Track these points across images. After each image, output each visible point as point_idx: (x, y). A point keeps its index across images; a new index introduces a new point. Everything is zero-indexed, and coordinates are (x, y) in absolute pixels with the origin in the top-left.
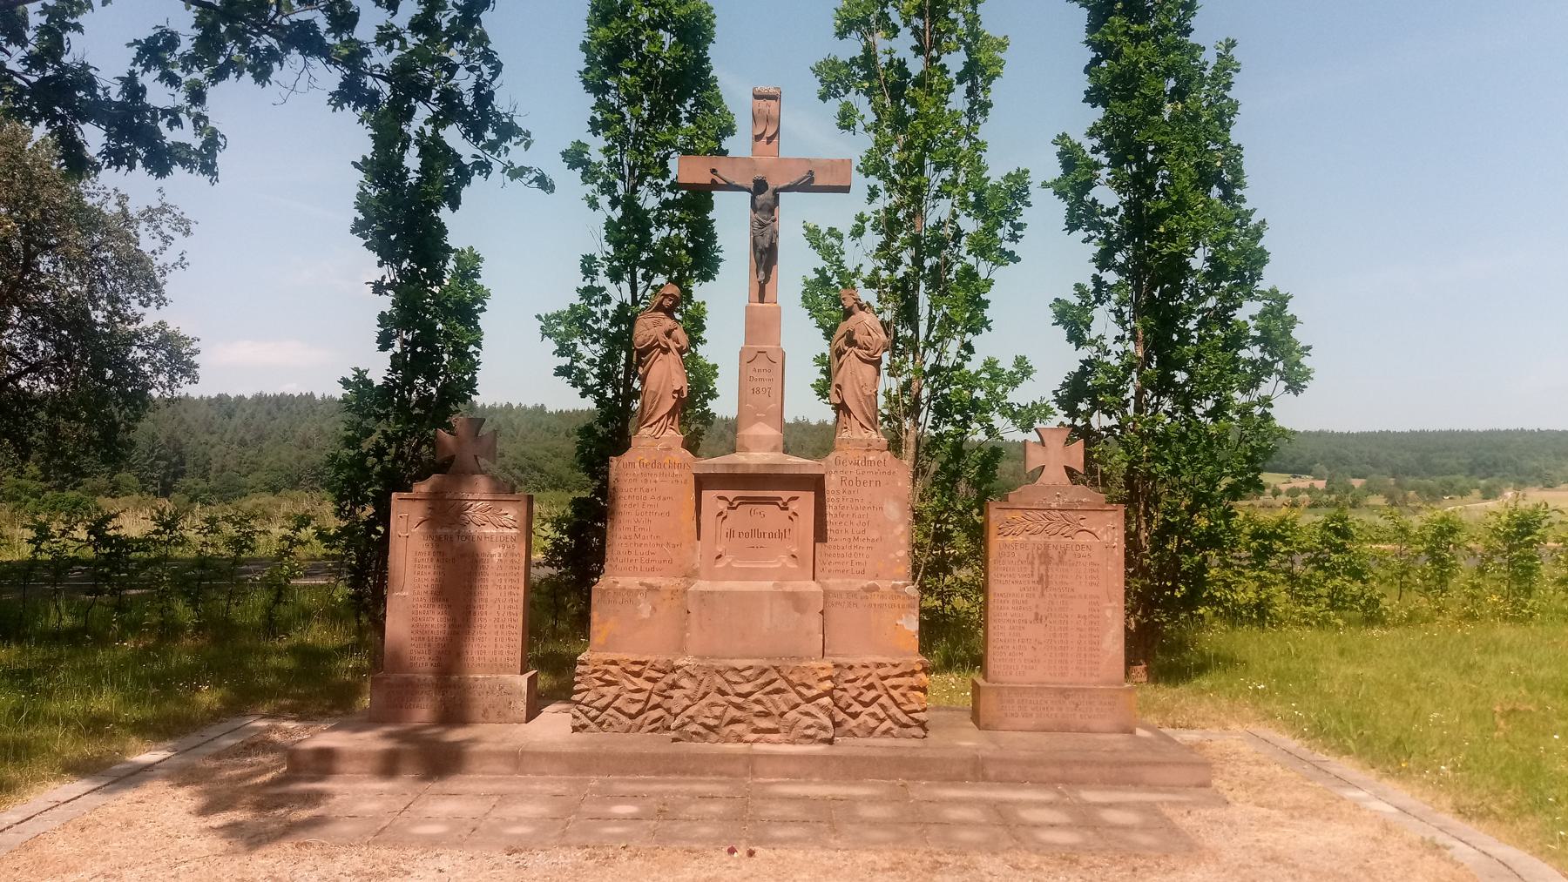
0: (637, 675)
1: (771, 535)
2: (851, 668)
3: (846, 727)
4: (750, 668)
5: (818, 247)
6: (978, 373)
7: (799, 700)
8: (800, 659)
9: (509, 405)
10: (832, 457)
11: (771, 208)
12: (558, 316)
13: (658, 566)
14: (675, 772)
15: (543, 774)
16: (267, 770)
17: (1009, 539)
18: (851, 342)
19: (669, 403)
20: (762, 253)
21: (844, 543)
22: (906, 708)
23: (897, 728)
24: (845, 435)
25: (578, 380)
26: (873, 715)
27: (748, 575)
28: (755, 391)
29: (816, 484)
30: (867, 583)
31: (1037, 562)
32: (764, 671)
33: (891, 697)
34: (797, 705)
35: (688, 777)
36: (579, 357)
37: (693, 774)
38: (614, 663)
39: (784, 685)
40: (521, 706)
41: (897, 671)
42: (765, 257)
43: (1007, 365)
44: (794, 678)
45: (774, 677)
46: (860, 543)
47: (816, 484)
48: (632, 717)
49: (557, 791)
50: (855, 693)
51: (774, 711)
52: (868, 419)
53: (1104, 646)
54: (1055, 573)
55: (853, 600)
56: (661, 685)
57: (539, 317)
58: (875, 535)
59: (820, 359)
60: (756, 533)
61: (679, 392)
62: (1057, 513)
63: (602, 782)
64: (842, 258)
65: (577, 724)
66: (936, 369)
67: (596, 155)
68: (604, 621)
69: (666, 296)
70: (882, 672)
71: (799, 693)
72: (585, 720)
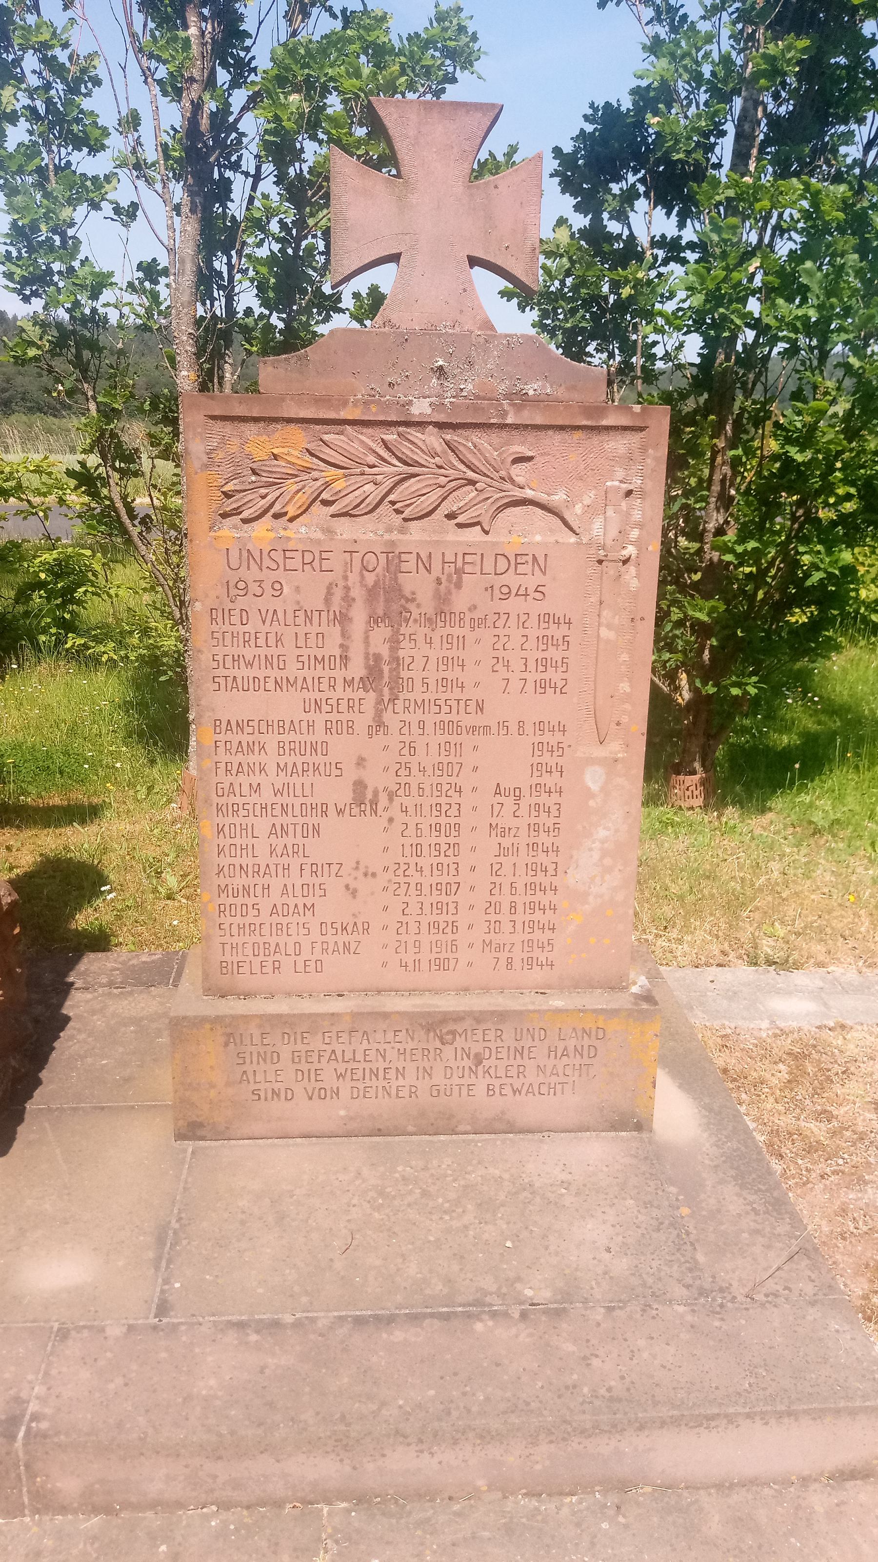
16: (362, 442)
17: (262, 532)
31: (359, 615)
53: (574, 878)
54: (421, 653)
62: (432, 439)
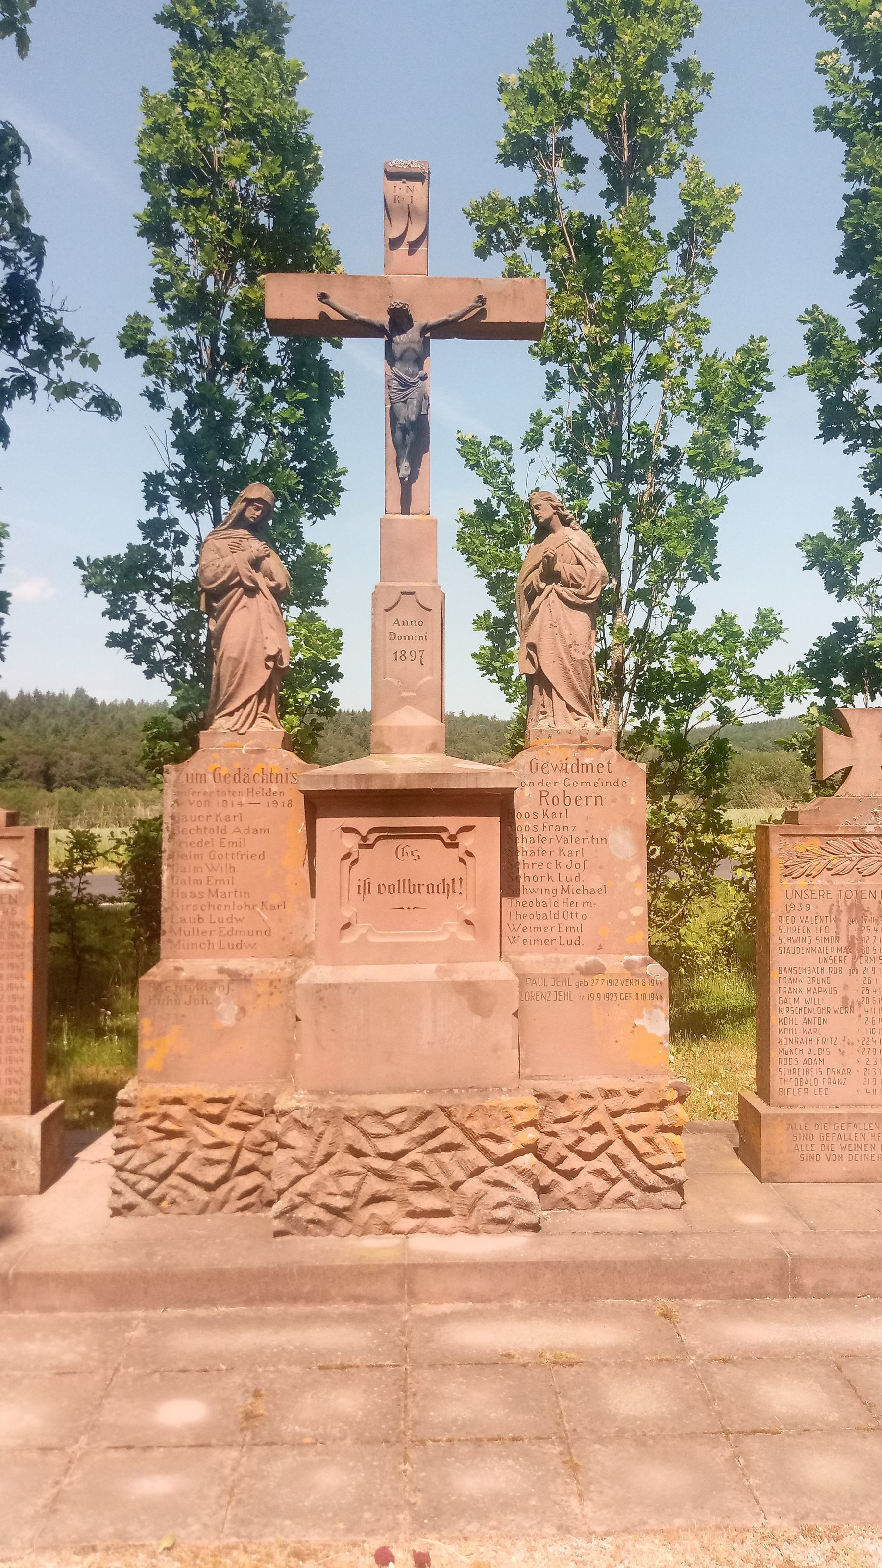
0: (217, 1119)
1: (432, 889)
2: (563, 1099)
3: (557, 1193)
4: (402, 1110)
5: (475, 466)
6: (710, 631)
7: (483, 1161)
8: (483, 1091)
9: (130, 702)
10: (523, 758)
11: (419, 358)
12: (108, 561)
13: (247, 939)
14: (278, 1298)
15: (52, 1309)
17: (801, 883)
18: (550, 575)
19: (260, 677)
20: (405, 431)
21: (546, 897)
22: (653, 1161)
23: (638, 1193)
24: (544, 724)
25: (142, 653)
26: (600, 1173)
27: (396, 954)
28: (400, 656)
29: (499, 804)
30: (584, 959)
31: (844, 918)
32: (425, 1115)
33: (629, 1144)
34: (480, 1170)
35: (302, 1308)
36: (141, 621)
37: (309, 1299)
38: (177, 1101)
39: (453, 1135)
40: (32, 1167)
41: (638, 1102)
42: (410, 437)
43: (746, 624)
44: (476, 1125)
45: (440, 1126)
46: (572, 897)
47: (499, 804)
48: (210, 1188)
49: (68, 1358)
50: (570, 1139)
51: (442, 1180)
52: (579, 698)
55: (564, 988)
56: (256, 1135)
57: (79, 563)
58: (595, 882)
59: (482, 622)
60: (407, 886)
61: (276, 658)
63: (152, 1327)
64: (512, 478)
65: (119, 1203)
66: (642, 633)
67: (161, 333)
68: (161, 1034)
69: (250, 502)
70: (613, 1104)
71: (484, 1151)
72: (130, 1197)
